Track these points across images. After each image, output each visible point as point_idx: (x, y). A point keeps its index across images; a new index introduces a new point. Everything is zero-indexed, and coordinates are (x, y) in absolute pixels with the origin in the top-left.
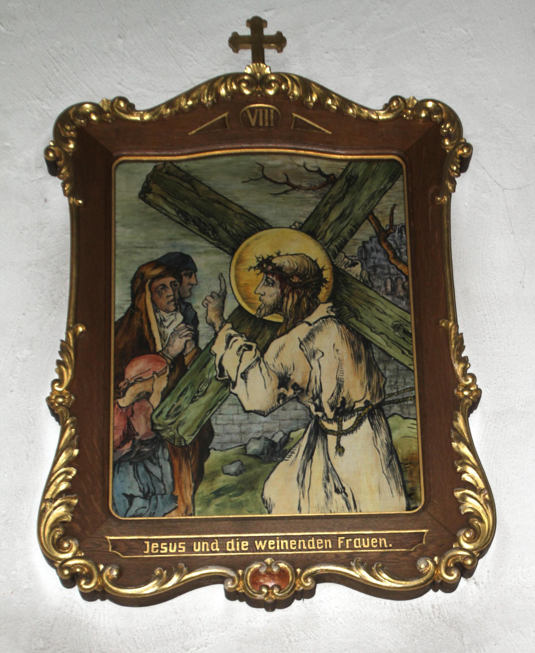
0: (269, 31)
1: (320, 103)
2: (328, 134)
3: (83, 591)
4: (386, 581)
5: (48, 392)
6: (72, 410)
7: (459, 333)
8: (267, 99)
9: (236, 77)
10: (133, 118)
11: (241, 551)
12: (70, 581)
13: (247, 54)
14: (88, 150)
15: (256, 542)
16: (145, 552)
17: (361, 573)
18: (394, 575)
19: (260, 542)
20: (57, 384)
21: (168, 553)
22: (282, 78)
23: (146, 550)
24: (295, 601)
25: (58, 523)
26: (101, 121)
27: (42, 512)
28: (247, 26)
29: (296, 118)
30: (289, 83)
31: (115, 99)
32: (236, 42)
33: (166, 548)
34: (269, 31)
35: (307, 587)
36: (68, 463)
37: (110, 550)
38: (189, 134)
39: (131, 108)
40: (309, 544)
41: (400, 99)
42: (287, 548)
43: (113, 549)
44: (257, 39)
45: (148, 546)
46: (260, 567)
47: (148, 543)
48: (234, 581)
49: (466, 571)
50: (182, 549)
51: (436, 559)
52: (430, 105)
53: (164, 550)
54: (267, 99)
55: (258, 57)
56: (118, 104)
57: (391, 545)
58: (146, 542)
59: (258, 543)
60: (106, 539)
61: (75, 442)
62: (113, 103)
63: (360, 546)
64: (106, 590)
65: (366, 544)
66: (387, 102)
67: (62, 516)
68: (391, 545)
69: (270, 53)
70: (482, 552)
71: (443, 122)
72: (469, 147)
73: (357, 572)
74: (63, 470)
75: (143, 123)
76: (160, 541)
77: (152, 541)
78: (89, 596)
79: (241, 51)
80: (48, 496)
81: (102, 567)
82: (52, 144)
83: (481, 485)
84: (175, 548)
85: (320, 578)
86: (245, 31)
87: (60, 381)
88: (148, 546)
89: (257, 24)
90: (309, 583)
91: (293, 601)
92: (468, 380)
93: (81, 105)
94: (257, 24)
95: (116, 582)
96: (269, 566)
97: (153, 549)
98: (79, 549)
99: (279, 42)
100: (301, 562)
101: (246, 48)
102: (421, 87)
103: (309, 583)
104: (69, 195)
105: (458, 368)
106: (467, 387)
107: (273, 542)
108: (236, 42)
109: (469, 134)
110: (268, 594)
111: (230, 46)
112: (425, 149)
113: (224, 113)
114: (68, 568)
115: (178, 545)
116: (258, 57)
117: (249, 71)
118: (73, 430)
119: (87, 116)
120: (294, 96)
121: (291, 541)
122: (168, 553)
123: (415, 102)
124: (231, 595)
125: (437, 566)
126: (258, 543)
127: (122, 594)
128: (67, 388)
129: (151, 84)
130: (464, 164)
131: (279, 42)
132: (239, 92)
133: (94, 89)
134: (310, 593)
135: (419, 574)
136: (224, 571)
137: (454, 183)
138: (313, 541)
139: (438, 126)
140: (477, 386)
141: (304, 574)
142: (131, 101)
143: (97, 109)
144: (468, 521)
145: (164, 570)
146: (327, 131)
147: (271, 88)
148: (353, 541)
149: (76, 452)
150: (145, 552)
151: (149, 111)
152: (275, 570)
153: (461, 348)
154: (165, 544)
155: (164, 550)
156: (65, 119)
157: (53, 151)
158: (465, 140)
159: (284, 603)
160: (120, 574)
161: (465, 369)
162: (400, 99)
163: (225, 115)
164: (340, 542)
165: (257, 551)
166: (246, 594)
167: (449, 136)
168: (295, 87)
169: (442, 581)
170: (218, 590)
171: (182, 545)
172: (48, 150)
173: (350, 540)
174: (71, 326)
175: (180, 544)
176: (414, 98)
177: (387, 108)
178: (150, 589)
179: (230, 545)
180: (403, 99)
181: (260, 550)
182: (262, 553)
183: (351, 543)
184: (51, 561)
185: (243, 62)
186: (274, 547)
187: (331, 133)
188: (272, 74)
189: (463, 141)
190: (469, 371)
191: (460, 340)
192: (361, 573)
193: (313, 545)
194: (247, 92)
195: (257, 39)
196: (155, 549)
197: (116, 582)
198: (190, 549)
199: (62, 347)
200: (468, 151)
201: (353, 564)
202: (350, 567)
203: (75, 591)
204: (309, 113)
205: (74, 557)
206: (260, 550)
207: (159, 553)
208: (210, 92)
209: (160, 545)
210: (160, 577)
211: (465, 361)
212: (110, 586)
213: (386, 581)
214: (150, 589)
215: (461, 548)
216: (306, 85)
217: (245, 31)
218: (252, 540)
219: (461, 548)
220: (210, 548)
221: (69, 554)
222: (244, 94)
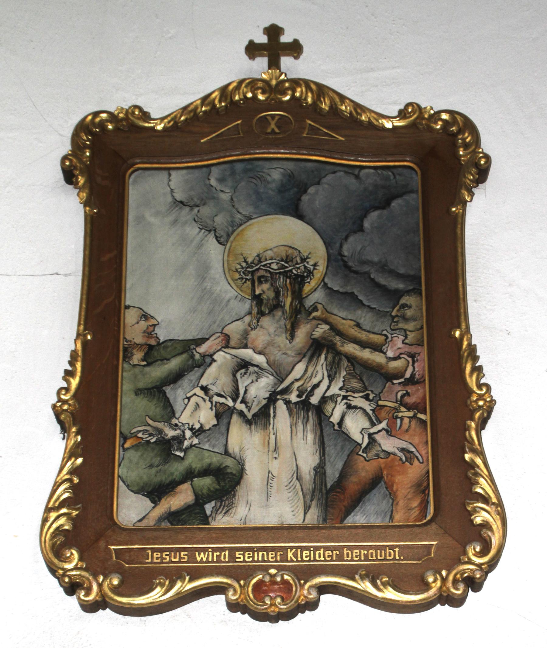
0: (285, 39)
1: (334, 109)
2: (341, 141)
3: (82, 602)
4: (390, 594)
5: (55, 400)
6: (76, 417)
7: (473, 344)
8: (280, 105)
9: (253, 84)
10: (147, 125)
11: (325, 560)
12: (71, 589)
13: (262, 62)
14: (107, 158)
15: (197, 553)
16: (146, 561)
17: (367, 586)
18: (397, 588)
19: (202, 553)
20: (63, 392)
21: (244, 561)
22: (296, 83)
23: (148, 559)
24: (439, 604)
25: (59, 531)
26: (117, 129)
27: (45, 520)
28: (264, 33)
29: (310, 125)
30: (304, 89)
31: (130, 107)
32: (253, 50)
33: (168, 557)
34: (285, 39)
35: (310, 599)
36: (72, 472)
37: (114, 559)
38: (202, 141)
39: (146, 116)
40: (350, 556)
41: (415, 105)
42: (266, 559)
43: (116, 558)
44: (274, 46)
45: (150, 554)
46: (263, 577)
47: (150, 552)
48: (235, 591)
49: (474, 584)
50: (184, 558)
51: (444, 573)
52: (445, 116)
53: (166, 559)
54: (280, 105)
55: (274, 64)
56: (133, 113)
57: (402, 558)
58: (148, 551)
59: (199, 555)
60: (110, 549)
61: (80, 451)
62: (129, 112)
63: (374, 558)
64: (107, 599)
65: (175, 557)
66: (402, 107)
67: (62, 525)
68: (402, 558)
69: (286, 62)
70: (492, 565)
71: (460, 131)
72: (488, 158)
73: (362, 584)
74: (66, 477)
75: (153, 129)
76: (162, 550)
77: (154, 550)
78: (90, 608)
79: (258, 60)
80: (51, 505)
81: (101, 578)
82: (70, 152)
83: (494, 500)
84: (178, 557)
85: (323, 589)
86: (263, 39)
87: (67, 390)
88: (150, 554)
89: (274, 32)
90: (313, 595)
91: (237, 612)
92: (482, 390)
93: (96, 114)
94: (274, 32)
95: (116, 590)
96: (272, 576)
97: (326, 556)
98: (81, 559)
99: (295, 49)
100: (305, 573)
101: (262, 55)
102: (438, 98)
103: (313, 595)
104: (86, 204)
105: (472, 382)
106: (481, 397)
107: (358, 551)
108: (253, 50)
109: (487, 145)
110: (271, 605)
111: (246, 54)
112: (440, 161)
113: (239, 120)
114: (69, 577)
115: (180, 555)
116: (274, 64)
117: (264, 76)
118: (79, 438)
119: (102, 125)
120: (307, 103)
121: (270, 553)
122: (244, 561)
123: (432, 112)
124: (233, 607)
125: (444, 580)
126: (199, 555)
127: (120, 602)
128: (74, 396)
129: (167, 87)
130: (482, 174)
131: (295, 49)
132: (255, 97)
133: (115, 98)
134: (312, 605)
135: (427, 586)
136: (225, 580)
137: (472, 194)
138: (322, 552)
139: (454, 136)
140: (492, 397)
141: (307, 586)
142: (145, 110)
143: (112, 117)
144: (479, 535)
145: (187, 576)
146: (340, 138)
147: (285, 94)
148: (220, 555)
149: (80, 461)
150: (146, 561)
151: (162, 119)
152: (279, 579)
153: (476, 358)
154: (242, 553)
155: (166, 559)
156: (82, 127)
157: (71, 161)
158: (483, 150)
159: (288, 616)
160: (122, 582)
161: (478, 380)
162: (415, 105)
163: (239, 122)
164: (290, 555)
165: (288, 561)
166: (247, 604)
167: (466, 146)
168: (310, 95)
169: (448, 595)
170: (220, 599)
171: (184, 555)
172: (65, 158)
173: (218, 554)
174: (81, 332)
175: (182, 553)
176: (432, 108)
177: (402, 114)
178: (156, 595)
179: (320, 554)
180: (418, 105)
181: (202, 561)
182: (294, 564)
183: (366, 556)
184: (53, 571)
185: (259, 67)
186: (275, 559)
187: (343, 139)
188: (288, 80)
189: (480, 150)
190: (482, 381)
191: (472, 349)
192: (367, 586)
193: (322, 556)
194: (261, 97)
195: (274, 46)
196: (157, 558)
197: (116, 590)
198: (192, 558)
199: (71, 356)
200: (486, 163)
201: (357, 577)
202: (353, 579)
203: (73, 601)
204: (326, 120)
205: (76, 568)
206: (202, 561)
207: (162, 563)
208: (223, 99)
209: (162, 556)
210: (162, 585)
211: (478, 370)
212: (112, 595)
213: (390, 594)
214: (156, 595)
215: (470, 562)
216: (321, 90)
217: (263, 39)
218: (232, 551)
219: (470, 562)
220: (324, 556)
221: (73, 560)
222: (259, 100)
